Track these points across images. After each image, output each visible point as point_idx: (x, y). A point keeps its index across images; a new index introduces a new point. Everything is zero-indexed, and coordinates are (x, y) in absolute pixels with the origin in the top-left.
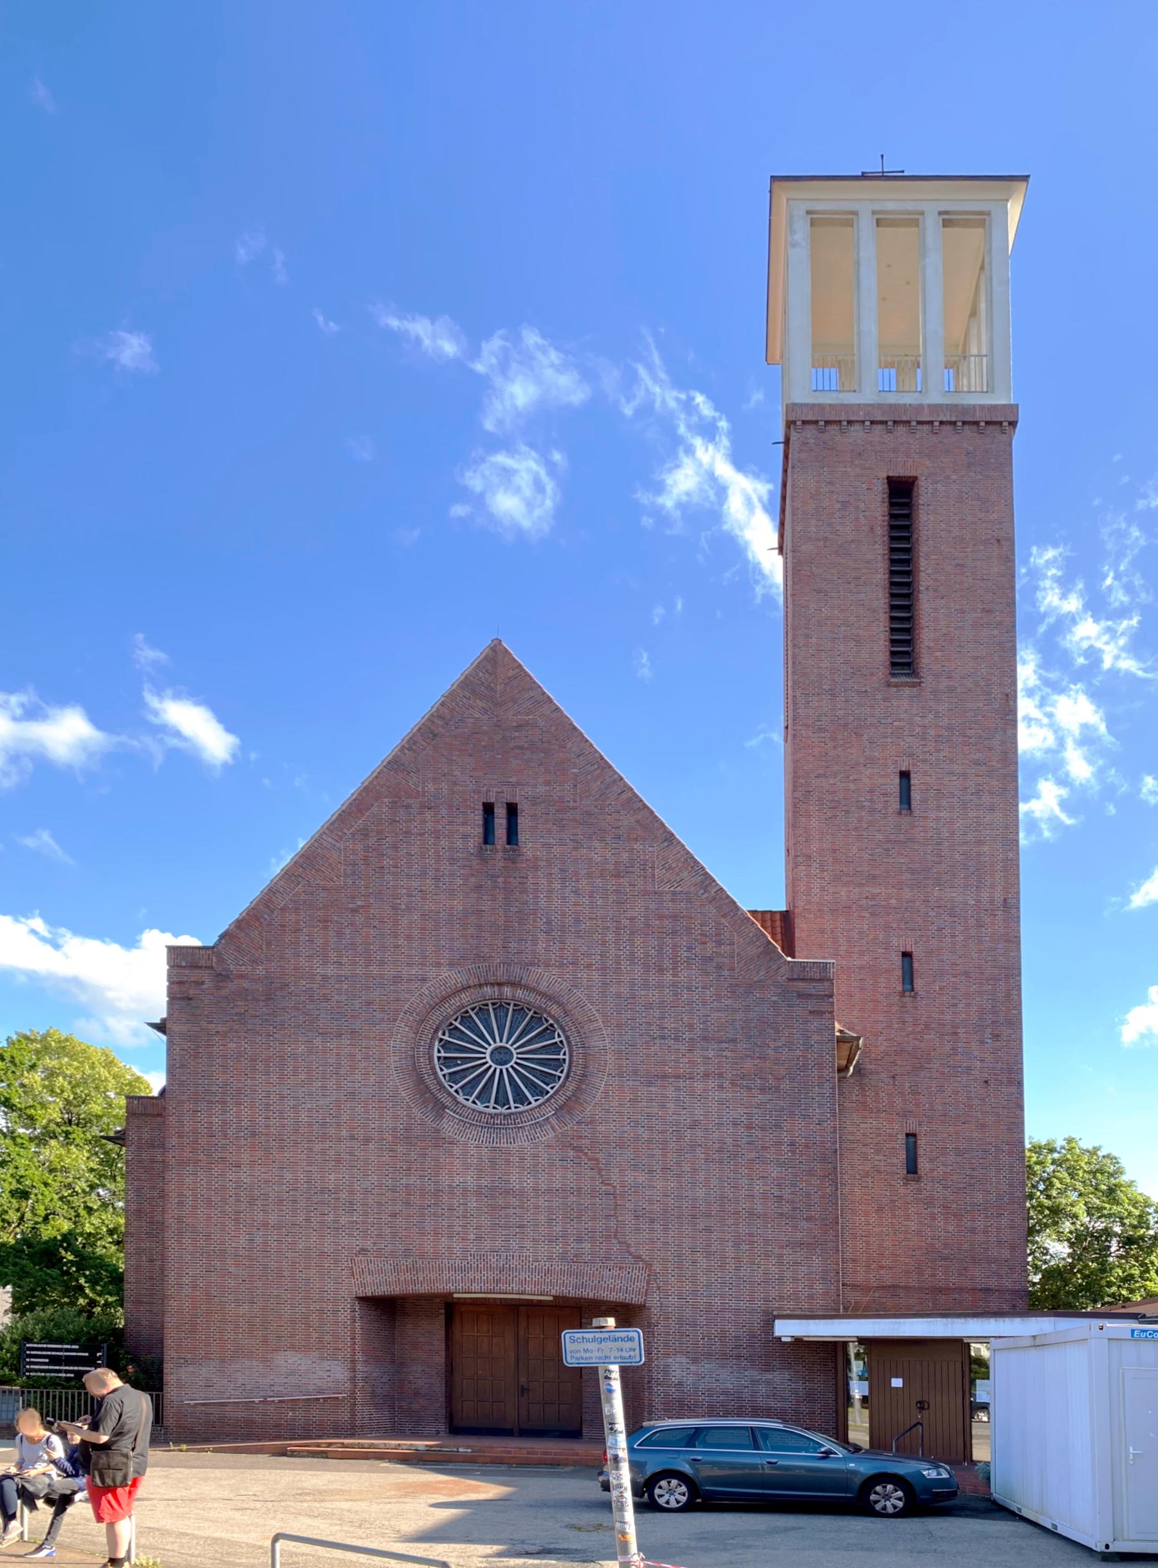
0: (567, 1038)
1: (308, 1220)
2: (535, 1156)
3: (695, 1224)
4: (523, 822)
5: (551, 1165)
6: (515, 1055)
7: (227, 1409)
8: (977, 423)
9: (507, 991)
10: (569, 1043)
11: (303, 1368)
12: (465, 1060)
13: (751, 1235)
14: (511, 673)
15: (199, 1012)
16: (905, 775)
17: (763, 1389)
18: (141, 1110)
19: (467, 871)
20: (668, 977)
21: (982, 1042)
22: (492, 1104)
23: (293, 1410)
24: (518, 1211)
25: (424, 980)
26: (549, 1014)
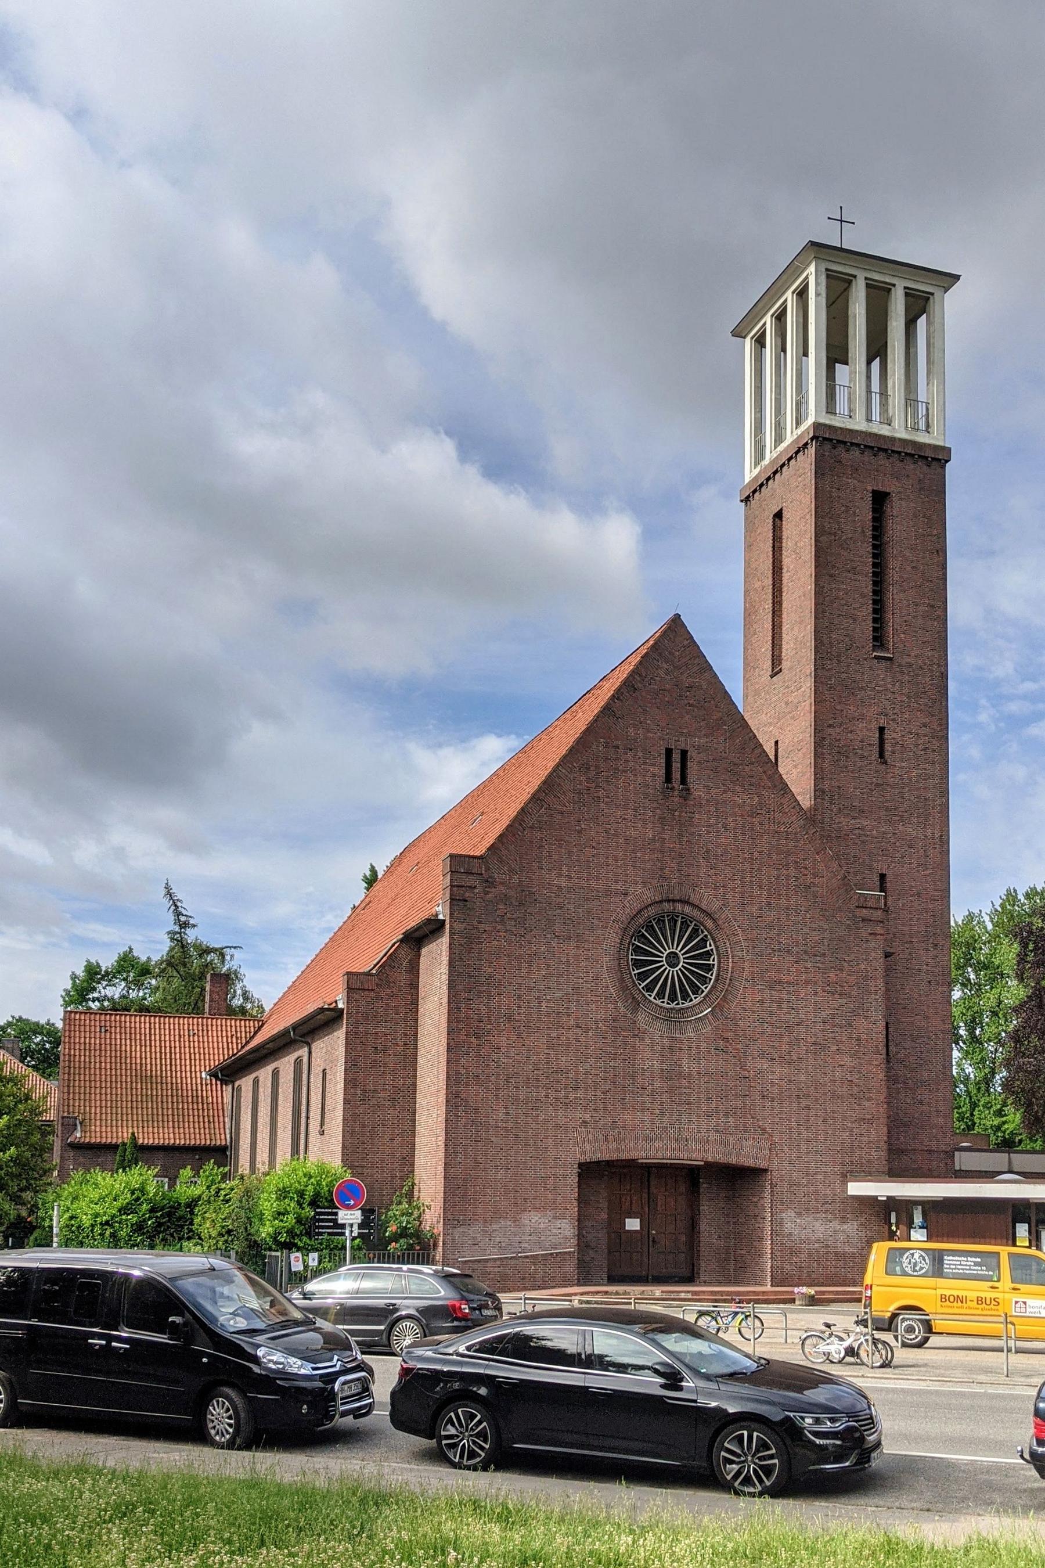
0: (717, 947)
1: (547, 1097)
2: (698, 1046)
3: (799, 1103)
4: (692, 767)
5: (709, 1052)
6: (682, 960)
7: (489, 1264)
8: (926, 458)
9: (679, 907)
10: (717, 950)
11: (542, 1226)
12: (692, 972)
13: (834, 1112)
14: (686, 643)
15: (472, 913)
16: (882, 730)
17: (841, 1237)
18: (358, 985)
19: (655, 805)
20: (783, 901)
21: (928, 950)
22: (666, 1000)
23: (534, 1264)
24: (687, 1091)
25: (626, 894)
26: (705, 927)
